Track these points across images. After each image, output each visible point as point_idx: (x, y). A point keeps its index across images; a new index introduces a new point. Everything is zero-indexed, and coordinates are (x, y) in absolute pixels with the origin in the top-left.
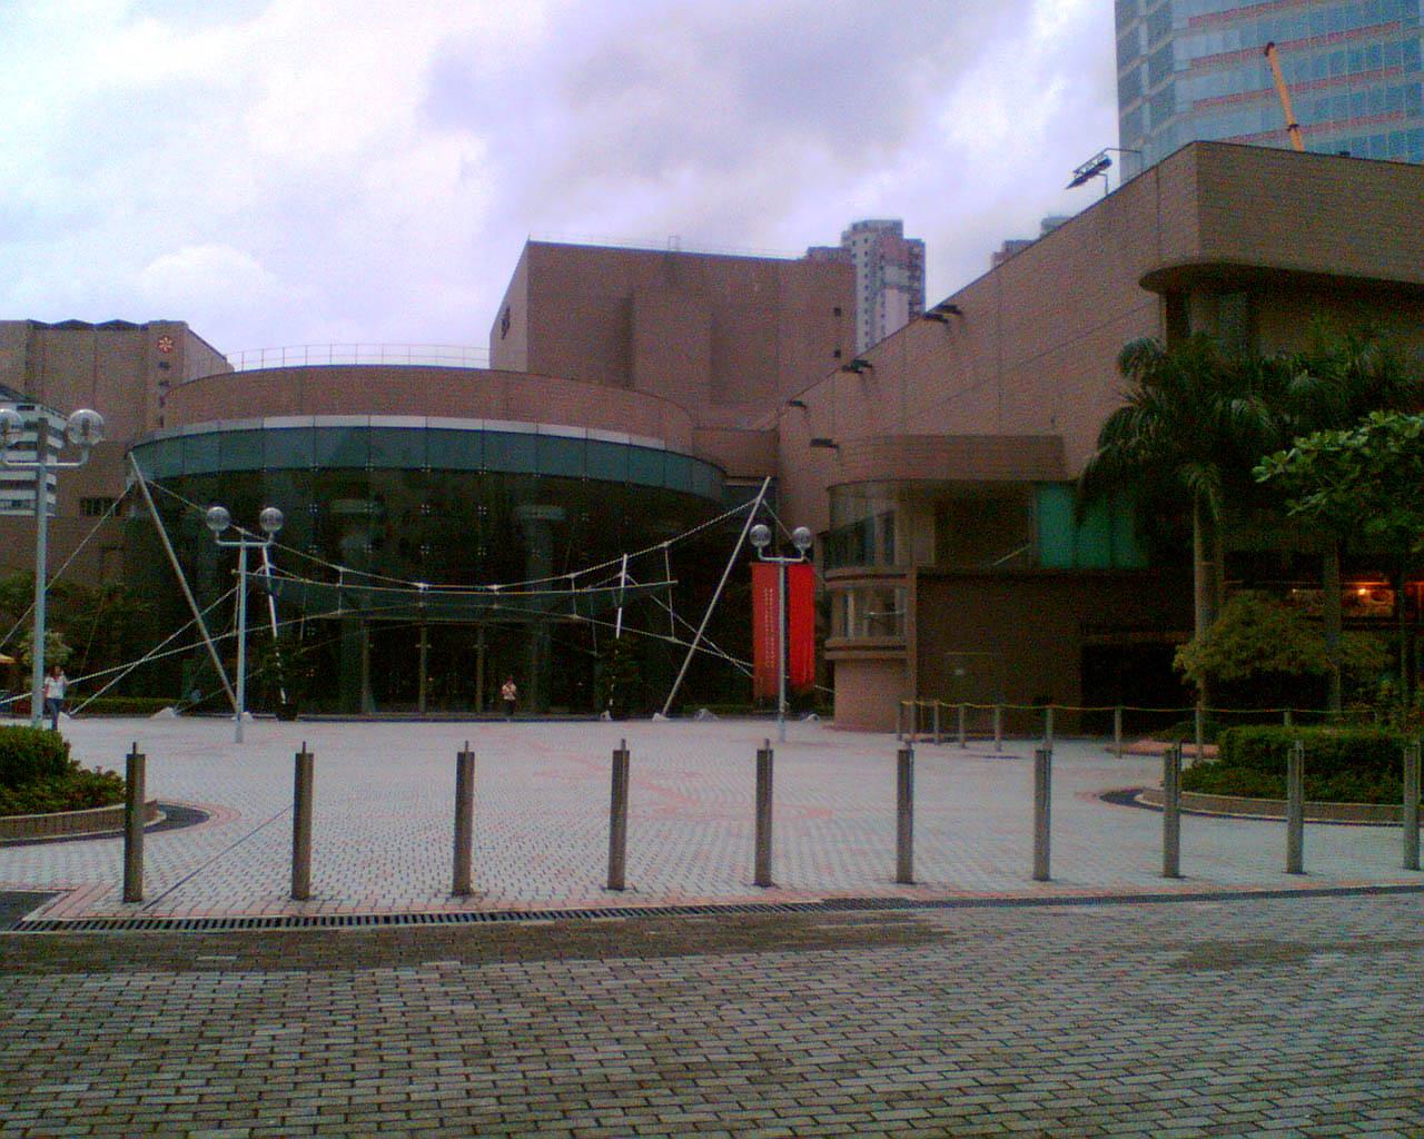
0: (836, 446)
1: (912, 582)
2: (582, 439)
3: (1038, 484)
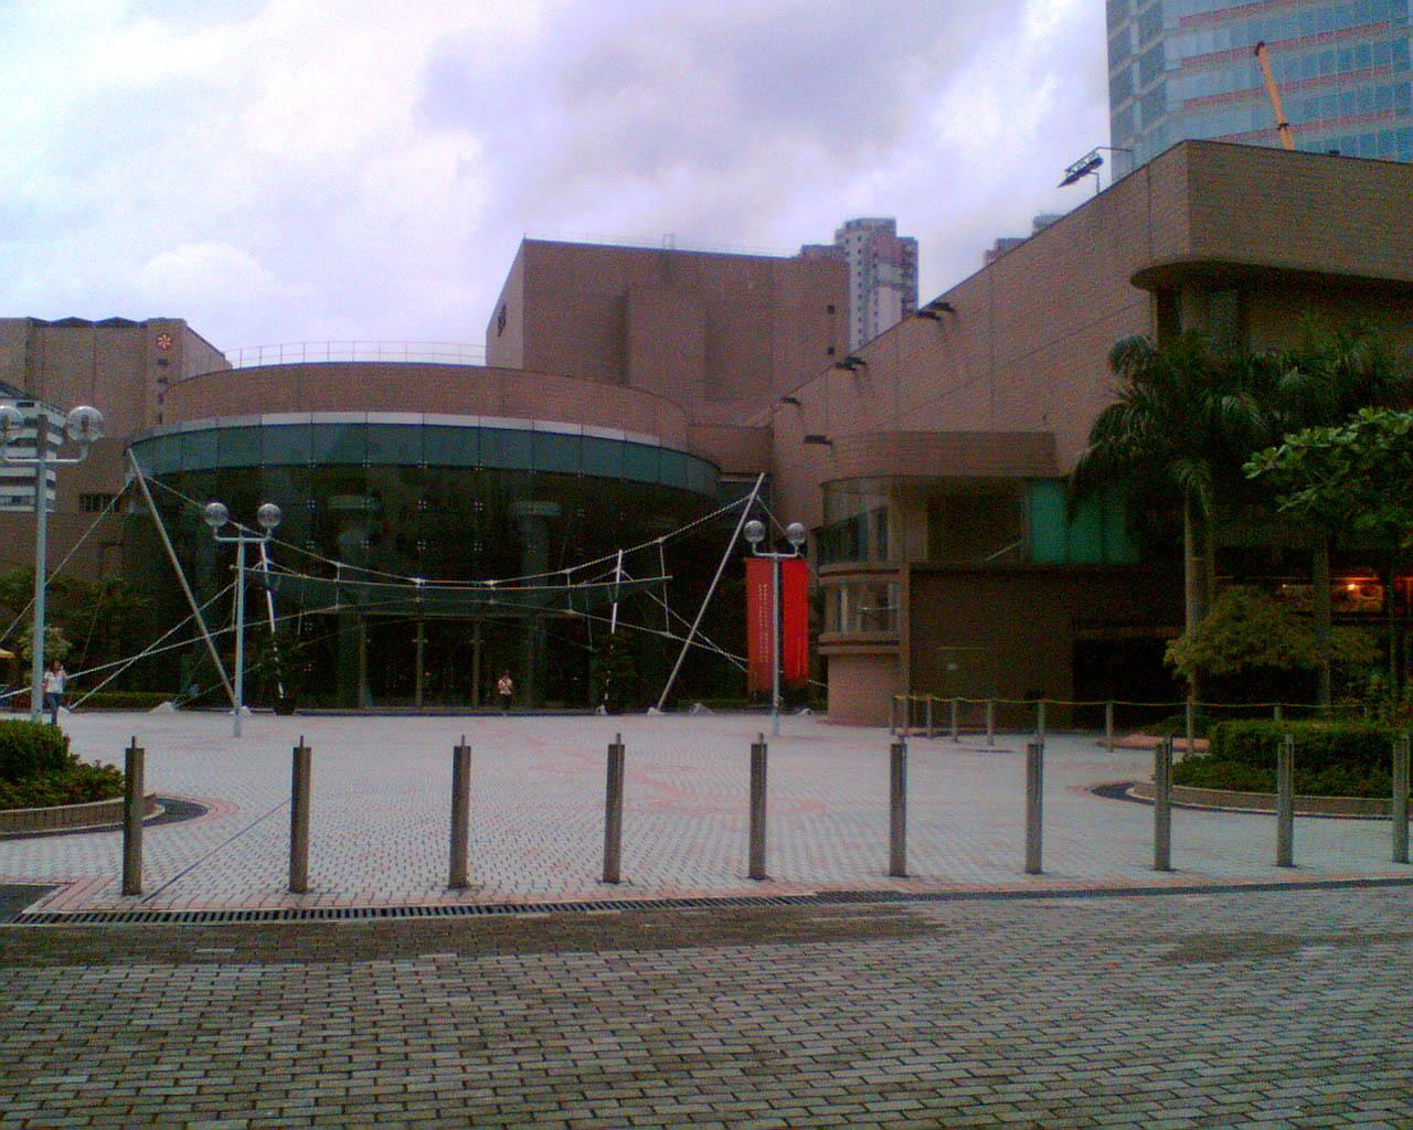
0: (829, 443)
1: (905, 577)
2: (578, 436)
3: (1030, 480)
